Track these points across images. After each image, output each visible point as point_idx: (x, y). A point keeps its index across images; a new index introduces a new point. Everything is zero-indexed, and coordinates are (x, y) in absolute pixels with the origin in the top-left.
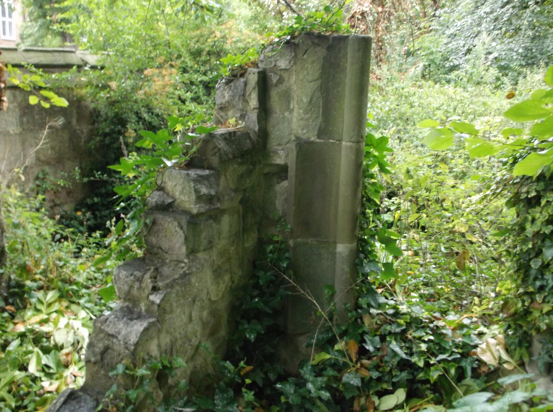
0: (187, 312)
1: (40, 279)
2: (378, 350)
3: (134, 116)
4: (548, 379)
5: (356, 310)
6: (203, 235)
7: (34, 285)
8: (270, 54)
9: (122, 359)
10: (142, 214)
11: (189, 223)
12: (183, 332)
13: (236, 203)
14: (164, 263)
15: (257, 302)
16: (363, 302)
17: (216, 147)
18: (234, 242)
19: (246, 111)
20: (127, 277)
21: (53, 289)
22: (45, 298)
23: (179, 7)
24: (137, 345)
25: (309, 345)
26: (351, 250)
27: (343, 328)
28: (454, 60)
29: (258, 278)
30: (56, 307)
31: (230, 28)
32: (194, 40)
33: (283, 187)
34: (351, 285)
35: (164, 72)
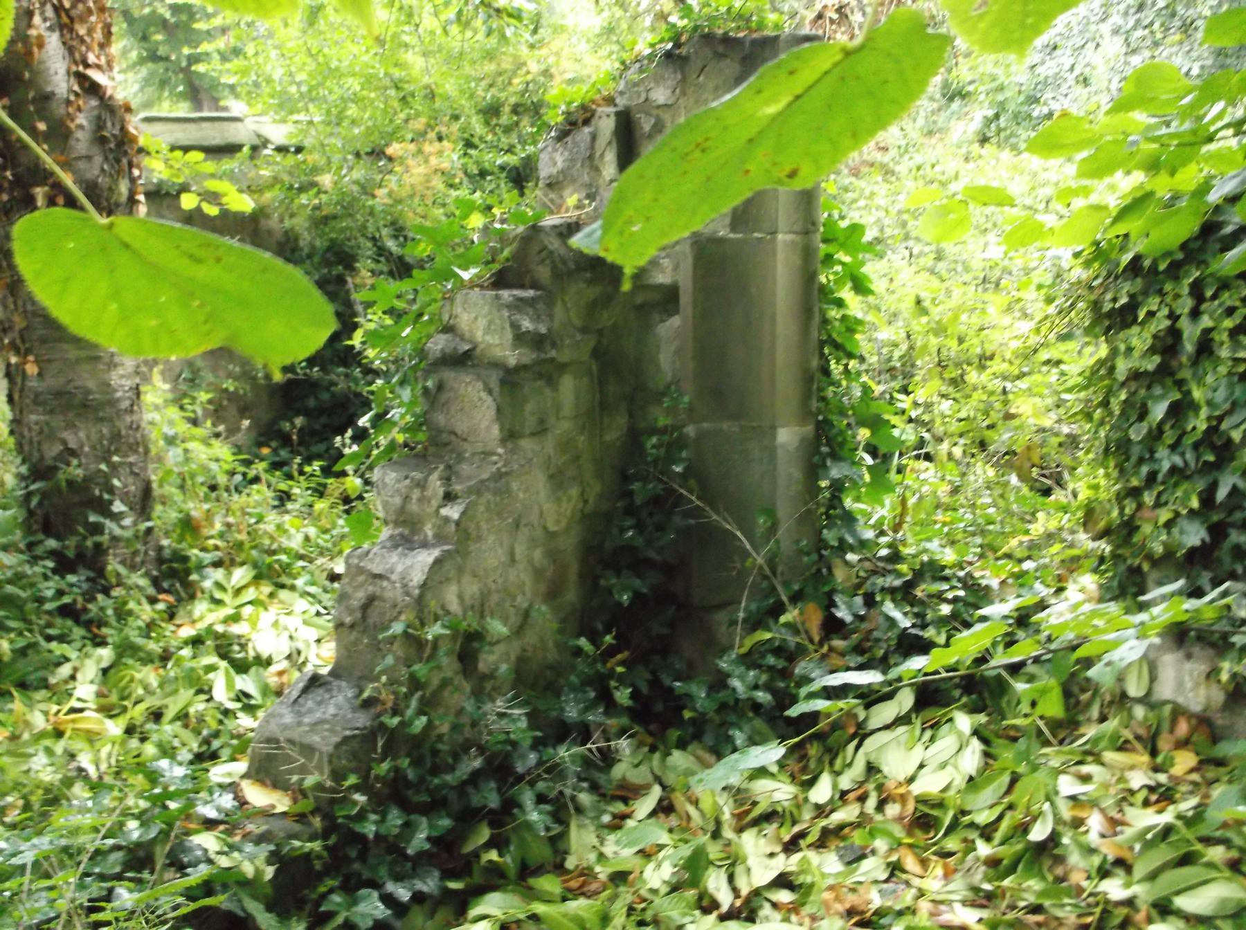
0: (506, 542)
1: (217, 548)
2: (861, 619)
3: (369, 244)
4: (1180, 654)
5: (818, 551)
6: (529, 407)
7: (208, 557)
8: (636, 77)
9: (400, 613)
10: (419, 374)
11: (503, 382)
12: (500, 581)
13: (584, 354)
14: (460, 458)
15: (631, 538)
16: (830, 536)
17: (545, 248)
18: (584, 427)
19: (597, 188)
20: (398, 481)
21: (243, 564)
22: (229, 580)
23: (451, 13)
24: (424, 586)
25: (733, 623)
26: (803, 440)
27: (796, 587)
28: (1051, 102)
29: (630, 494)
30: (250, 594)
31: (557, 54)
32: (483, 83)
33: (670, 328)
34: (806, 504)
35: (427, 148)
